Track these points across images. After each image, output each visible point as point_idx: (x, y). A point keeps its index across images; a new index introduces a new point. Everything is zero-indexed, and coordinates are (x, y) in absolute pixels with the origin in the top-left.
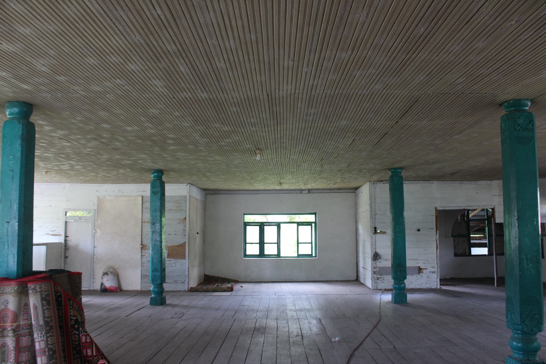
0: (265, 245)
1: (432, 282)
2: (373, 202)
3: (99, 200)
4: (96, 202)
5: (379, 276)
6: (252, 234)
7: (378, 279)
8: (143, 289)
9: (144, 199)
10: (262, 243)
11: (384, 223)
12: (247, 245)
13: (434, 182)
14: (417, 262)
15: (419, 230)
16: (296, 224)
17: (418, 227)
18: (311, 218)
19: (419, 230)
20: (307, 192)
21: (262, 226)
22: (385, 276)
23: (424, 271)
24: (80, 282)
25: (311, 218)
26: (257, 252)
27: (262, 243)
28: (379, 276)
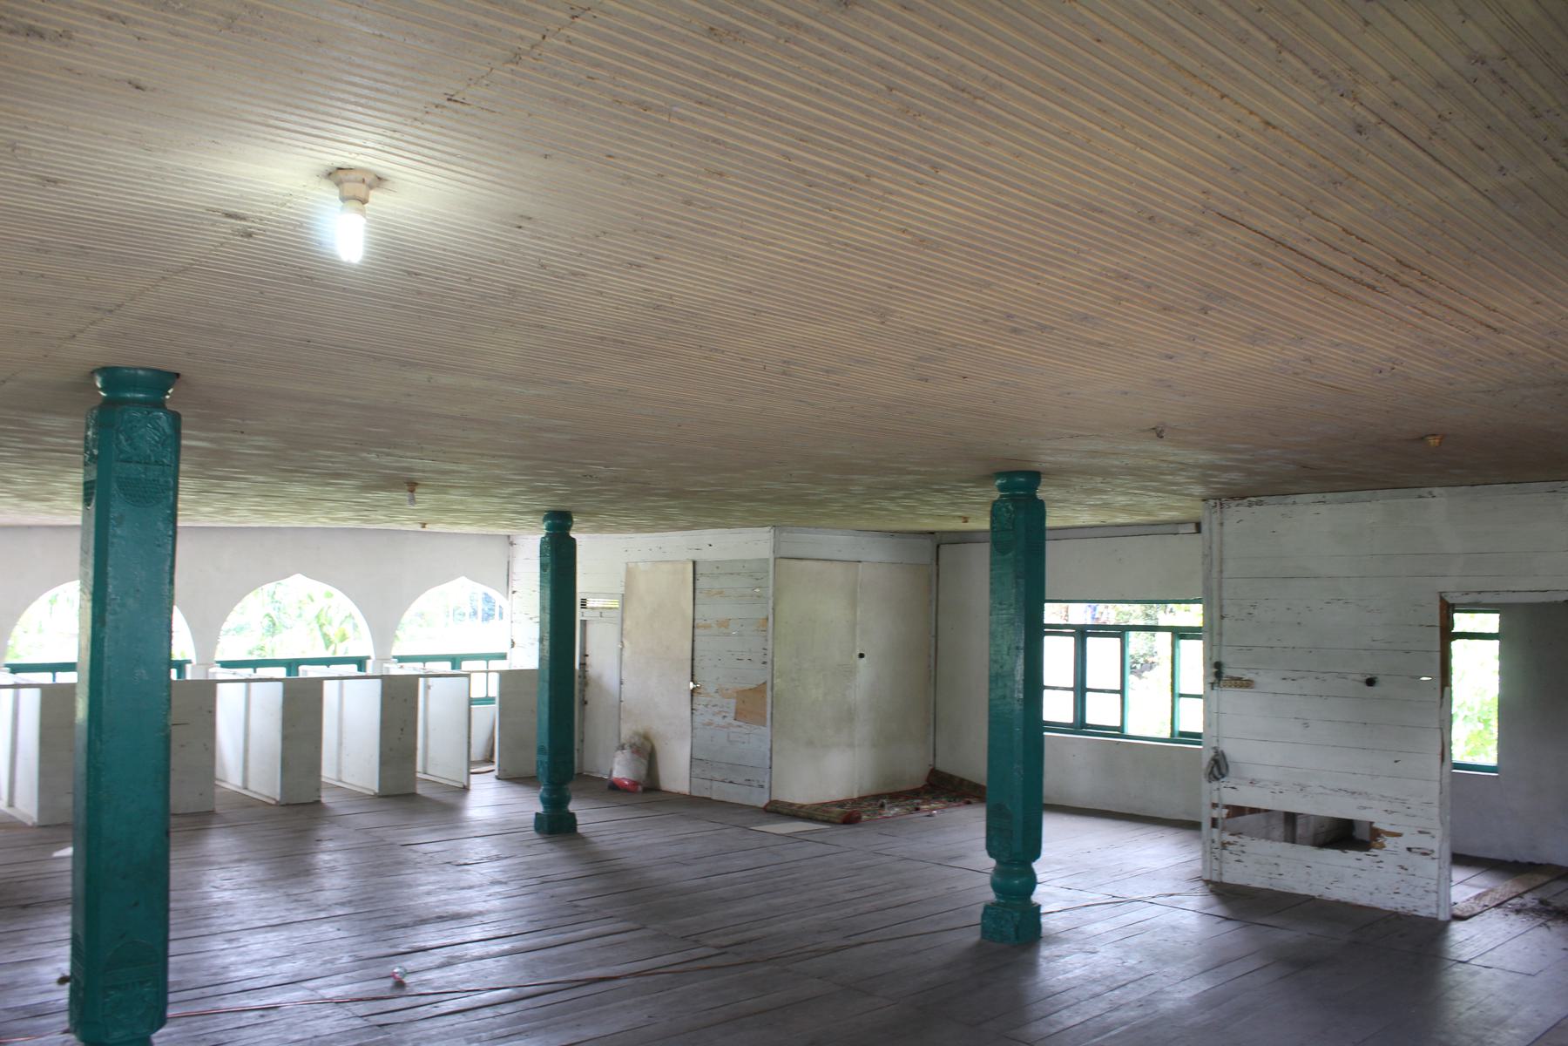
0: (1046, 692)
1: (1420, 892)
2: (1215, 574)
3: (630, 573)
4: (623, 573)
5: (1227, 838)
6: (1057, 656)
7: (1224, 845)
8: (695, 794)
9: (698, 568)
10: (1080, 690)
11: (1250, 648)
12: (1088, 694)
13: (1436, 491)
14: (1365, 803)
15: (1370, 682)
16: (1168, 635)
17: (1371, 671)
18: (1191, 615)
19: (1370, 682)
20: (1192, 528)
21: (1081, 634)
22: (1245, 840)
23: (1389, 842)
24: (1500, 739)
25: (1191, 615)
26: (1068, 718)
27: (1080, 690)
28: (1227, 838)
